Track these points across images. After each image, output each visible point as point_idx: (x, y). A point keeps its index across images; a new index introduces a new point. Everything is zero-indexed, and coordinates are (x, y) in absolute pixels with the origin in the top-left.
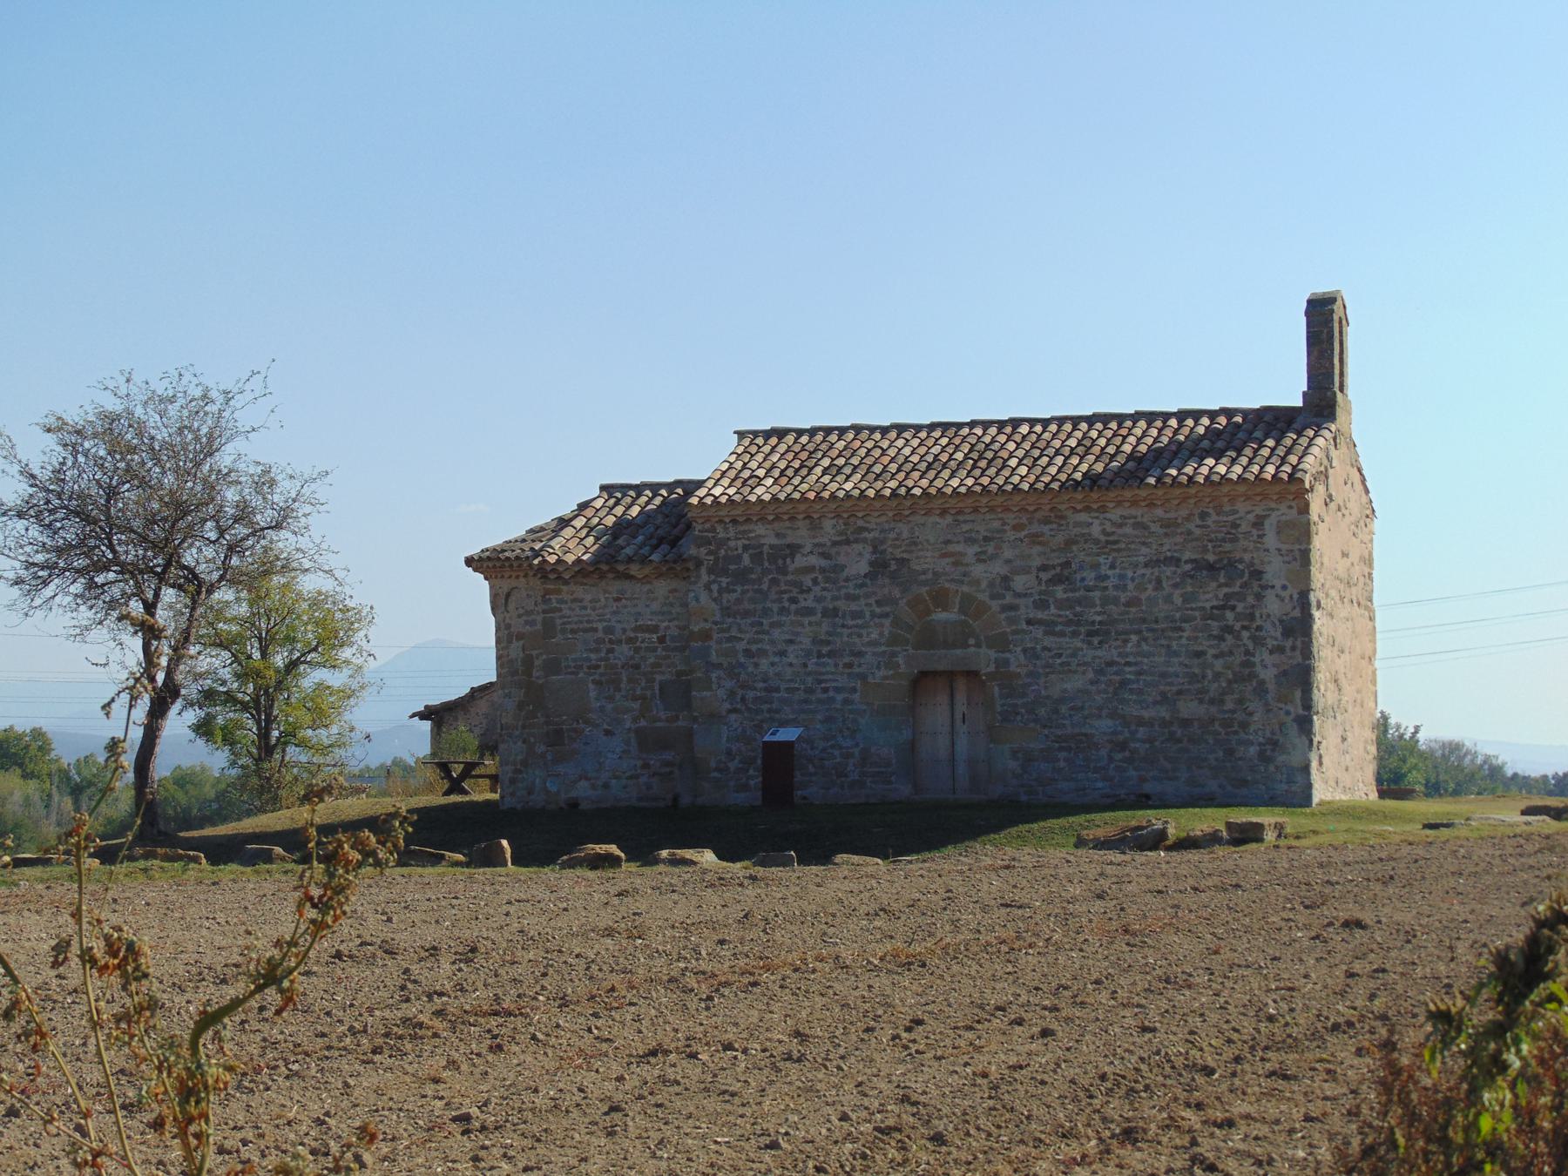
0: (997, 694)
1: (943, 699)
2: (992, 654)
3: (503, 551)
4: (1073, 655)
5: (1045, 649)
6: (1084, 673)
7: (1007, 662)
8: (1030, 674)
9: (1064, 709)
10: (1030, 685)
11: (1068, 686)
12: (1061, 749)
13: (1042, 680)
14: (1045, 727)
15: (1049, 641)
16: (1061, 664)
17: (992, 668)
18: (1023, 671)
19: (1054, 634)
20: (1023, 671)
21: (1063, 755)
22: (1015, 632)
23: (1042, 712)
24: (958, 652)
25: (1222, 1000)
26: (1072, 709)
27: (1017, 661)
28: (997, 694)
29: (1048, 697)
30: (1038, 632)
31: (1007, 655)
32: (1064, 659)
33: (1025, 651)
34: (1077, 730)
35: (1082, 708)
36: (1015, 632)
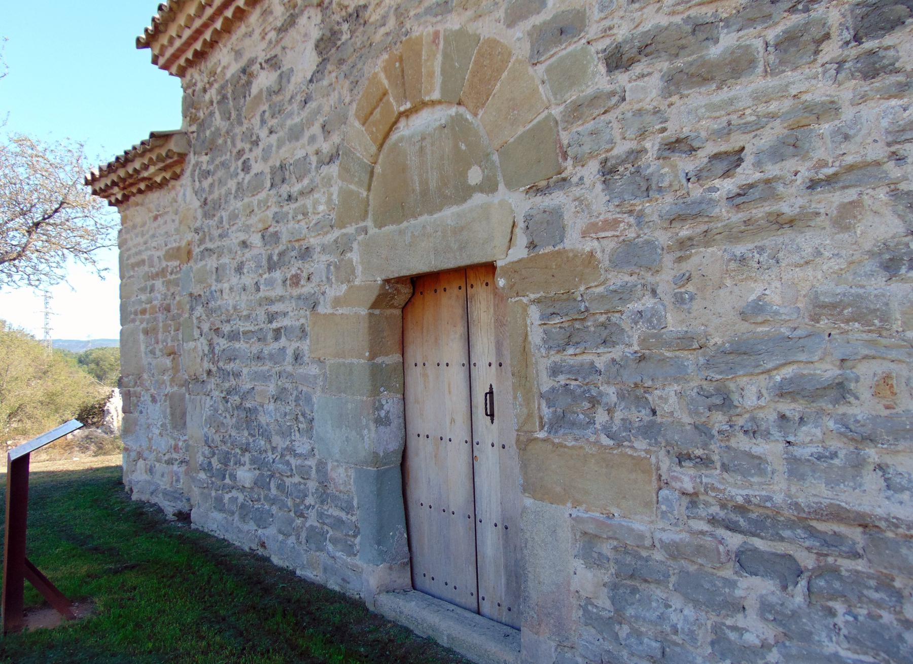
0: (536, 336)
1: (452, 349)
2: (519, 203)
3: (899, 215)
4: (792, 145)
5: (678, 145)
6: (845, 218)
7: (554, 219)
8: (633, 255)
9: (752, 392)
10: (624, 294)
11: (770, 289)
12: (745, 561)
13: (665, 280)
14: (682, 458)
15: (694, 111)
16: (739, 198)
17: (519, 252)
18: (602, 248)
19: (702, 76)
20: (602, 248)
21: (756, 588)
22: (576, 111)
23: (670, 400)
24: (449, 214)
25: (185, 585)
26: (784, 392)
27: (585, 209)
28: (536, 336)
29: (686, 342)
30: (644, 85)
31: (557, 198)
32: (747, 173)
33: (608, 171)
34: (816, 492)
35: (840, 390)
36: (576, 111)
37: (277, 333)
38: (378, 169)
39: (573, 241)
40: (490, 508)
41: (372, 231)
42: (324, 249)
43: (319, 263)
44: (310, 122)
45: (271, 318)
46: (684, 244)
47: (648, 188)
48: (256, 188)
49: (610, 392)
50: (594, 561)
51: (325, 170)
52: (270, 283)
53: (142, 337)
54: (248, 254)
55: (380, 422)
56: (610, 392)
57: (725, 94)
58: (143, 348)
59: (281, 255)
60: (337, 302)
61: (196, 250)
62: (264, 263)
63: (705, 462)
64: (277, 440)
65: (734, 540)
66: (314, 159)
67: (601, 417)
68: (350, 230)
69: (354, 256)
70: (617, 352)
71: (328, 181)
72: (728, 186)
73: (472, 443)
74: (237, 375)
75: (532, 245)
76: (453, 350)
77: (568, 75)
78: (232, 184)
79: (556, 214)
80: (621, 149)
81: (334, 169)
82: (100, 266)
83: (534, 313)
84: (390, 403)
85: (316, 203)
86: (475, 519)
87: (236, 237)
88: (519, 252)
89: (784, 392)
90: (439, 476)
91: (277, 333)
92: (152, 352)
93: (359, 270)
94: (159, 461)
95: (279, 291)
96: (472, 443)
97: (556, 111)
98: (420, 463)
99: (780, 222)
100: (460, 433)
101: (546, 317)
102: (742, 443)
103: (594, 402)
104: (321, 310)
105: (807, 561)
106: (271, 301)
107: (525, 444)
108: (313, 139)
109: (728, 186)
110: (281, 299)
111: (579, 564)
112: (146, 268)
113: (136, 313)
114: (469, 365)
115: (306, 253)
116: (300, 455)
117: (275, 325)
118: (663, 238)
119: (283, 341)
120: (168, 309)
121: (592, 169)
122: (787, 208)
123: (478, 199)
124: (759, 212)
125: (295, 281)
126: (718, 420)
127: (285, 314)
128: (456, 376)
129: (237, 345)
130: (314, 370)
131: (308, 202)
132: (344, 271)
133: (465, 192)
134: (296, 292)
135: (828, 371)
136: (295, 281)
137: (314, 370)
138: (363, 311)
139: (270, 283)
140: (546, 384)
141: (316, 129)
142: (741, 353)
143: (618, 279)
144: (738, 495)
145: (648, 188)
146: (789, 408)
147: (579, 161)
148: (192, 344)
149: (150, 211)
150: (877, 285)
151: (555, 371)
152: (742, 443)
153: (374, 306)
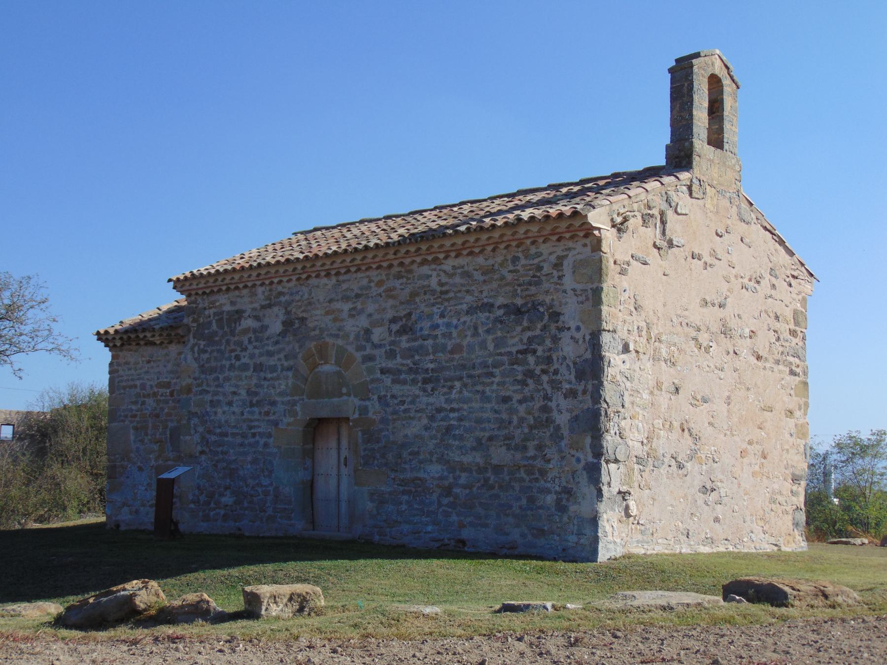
0: (360, 440)
4: (413, 402)
6: (420, 419)
8: (383, 421)
9: (405, 454)
12: (404, 493)
17: (356, 416)
26: (410, 454)
27: (374, 409)
28: (360, 440)
31: (367, 403)
32: (406, 406)
33: (380, 398)
37: (254, 435)
38: (309, 379)
39: (370, 415)
40: (344, 495)
41: (306, 400)
42: (283, 403)
43: (281, 408)
44: (279, 352)
45: (250, 428)
46: (394, 420)
47: (388, 405)
48: (245, 368)
49: (378, 455)
50: (372, 501)
51: (285, 373)
52: (252, 413)
53: (132, 431)
54: (236, 398)
55: (305, 469)
56: (378, 455)
57: (402, 388)
58: (132, 438)
59: (257, 401)
60: (289, 424)
61: (194, 389)
62: (248, 404)
63: (396, 471)
64: (251, 482)
65: (401, 488)
66: (280, 367)
67: (376, 462)
68: (296, 398)
69: (298, 408)
70: (380, 445)
71: (287, 378)
72: (403, 408)
73: (339, 475)
74: (226, 453)
75: (360, 414)
76: (333, 444)
77: (370, 371)
78: (227, 363)
79: (366, 407)
80: (383, 393)
81: (290, 374)
82: (16, 368)
83: (360, 434)
84: (309, 462)
85: (280, 384)
86: (338, 500)
87: (228, 388)
88: (356, 416)
89: (410, 454)
90: (326, 486)
91: (254, 435)
92: (142, 441)
93: (300, 413)
94: (143, 505)
95: (256, 417)
96: (339, 475)
97: (368, 379)
98: (320, 483)
99: (411, 418)
100: (334, 472)
101: (363, 435)
102: (403, 466)
103: (374, 458)
104: (280, 426)
105: (414, 490)
106: (251, 421)
107: (356, 470)
108: (279, 359)
109: (403, 408)
110: (258, 420)
111: (369, 503)
112: (138, 390)
113: (126, 416)
114: (339, 449)
115: (273, 403)
116: (265, 486)
117: (252, 431)
118: (390, 417)
119: (257, 438)
120: (157, 416)
121: (375, 397)
122: (412, 415)
123: (345, 398)
124: (407, 415)
125: (267, 413)
126: (399, 461)
127: (259, 427)
128: (334, 453)
129: (226, 439)
130: (275, 450)
131: (276, 383)
132: (294, 414)
133: (341, 395)
134: (267, 418)
135: (416, 449)
136: (267, 413)
137: (275, 450)
138: (301, 429)
139: (252, 413)
140: (362, 454)
141: (282, 356)
142: (404, 446)
143: (381, 426)
144: (402, 477)
145: (388, 405)
146: (411, 457)
147: (373, 394)
148: (188, 438)
149: (143, 356)
150: (424, 433)
151: (365, 450)
152: (403, 466)
153: (305, 427)
